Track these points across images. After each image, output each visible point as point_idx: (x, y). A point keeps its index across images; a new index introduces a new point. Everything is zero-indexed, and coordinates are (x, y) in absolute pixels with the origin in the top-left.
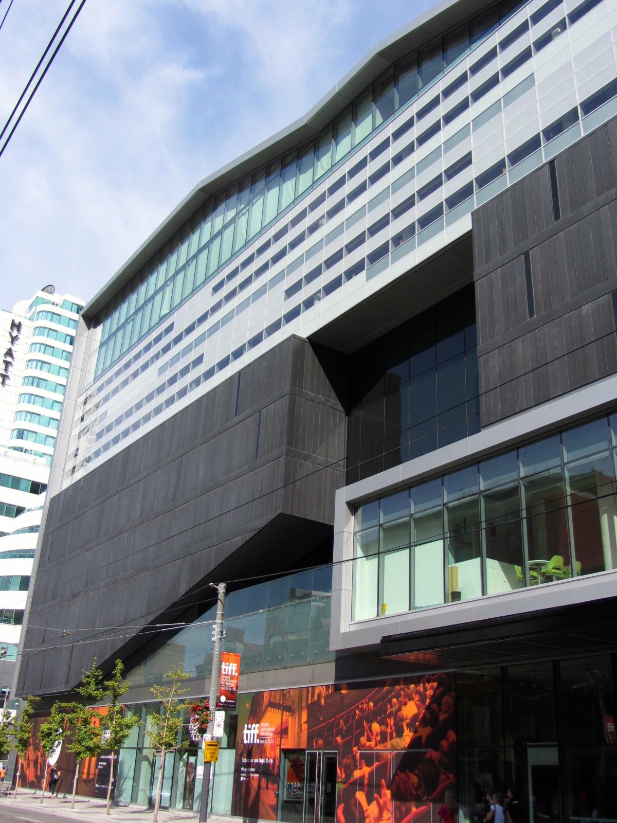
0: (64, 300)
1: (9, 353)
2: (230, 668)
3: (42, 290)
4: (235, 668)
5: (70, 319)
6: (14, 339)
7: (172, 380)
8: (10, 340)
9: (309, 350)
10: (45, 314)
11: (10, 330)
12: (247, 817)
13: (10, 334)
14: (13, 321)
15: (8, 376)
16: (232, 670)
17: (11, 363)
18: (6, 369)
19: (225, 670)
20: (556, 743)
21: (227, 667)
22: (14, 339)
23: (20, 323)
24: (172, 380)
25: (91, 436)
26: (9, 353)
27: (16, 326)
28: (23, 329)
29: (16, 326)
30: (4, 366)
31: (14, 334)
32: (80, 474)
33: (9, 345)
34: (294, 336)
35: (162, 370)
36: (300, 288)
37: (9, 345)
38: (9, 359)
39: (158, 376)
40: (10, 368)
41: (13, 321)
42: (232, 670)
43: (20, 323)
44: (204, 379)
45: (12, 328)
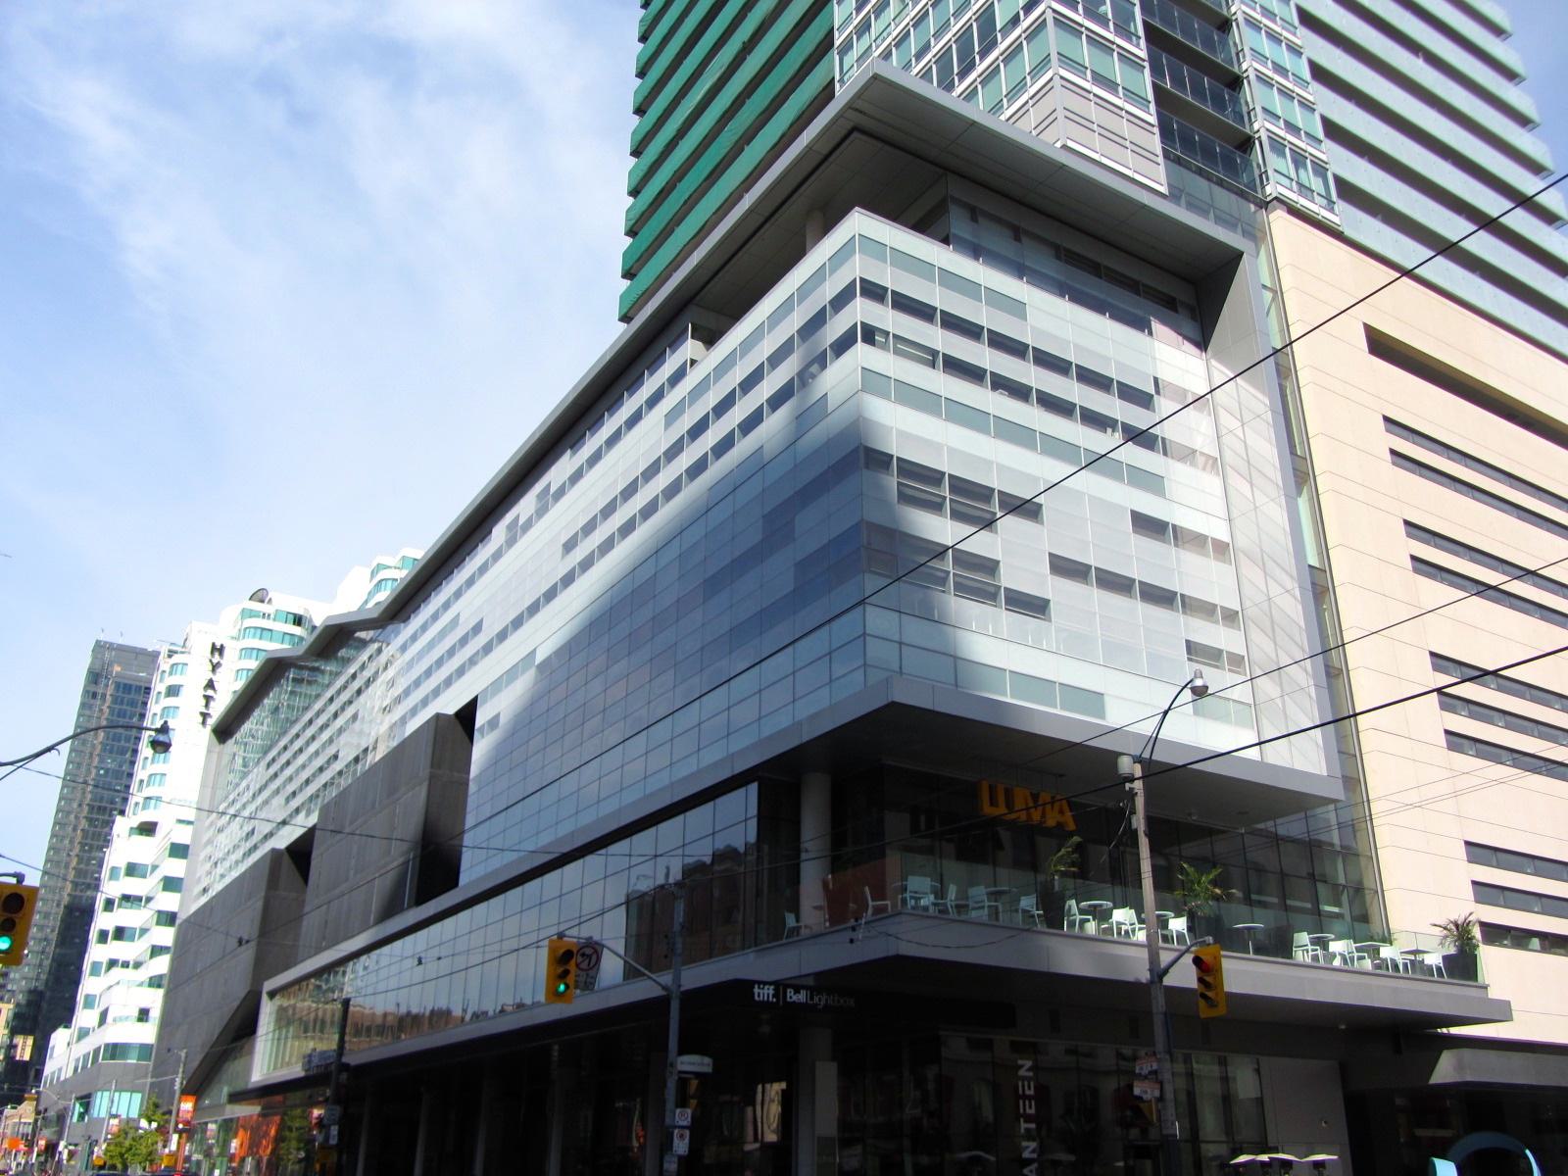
0: (277, 611)
1: (210, 685)
2: (766, 991)
3: (250, 599)
4: (771, 992)
5: (285, 633)
6: (215, 667)
7: (698, 430)
8: (211, 668)
9: (287, 859)
10: (252, 630)
11: (209, 655)
12: (23, 1096)
13: (211, 661)
14: (214, 645)
15: (209, 714)
16: (768, 995)
17: (212, 697)
18: (207, 705)
19: (759, 994)
20: (760, 1087)
21: (761, 991)
22: (215, 667)
23: (222, 646)
24: (698, 430)
25: (279, 800)
26: (210, 685)
27: (218, 650)
28: (226, 652)
29: (218, 650)
30: (204, 702)
31: (215, 661)
32: (227, 880)
33: (210, 675)
34: (438, 716)
35: (671, 418)
36: (762, 378)
37: (210, 675)
38: (210, 692)
39: (666, 428)
40: (212, 704)
41: (214, 645)
42: (768, 995)
43: (222, 646)
44: (714, 458)
45: (212, 653)
